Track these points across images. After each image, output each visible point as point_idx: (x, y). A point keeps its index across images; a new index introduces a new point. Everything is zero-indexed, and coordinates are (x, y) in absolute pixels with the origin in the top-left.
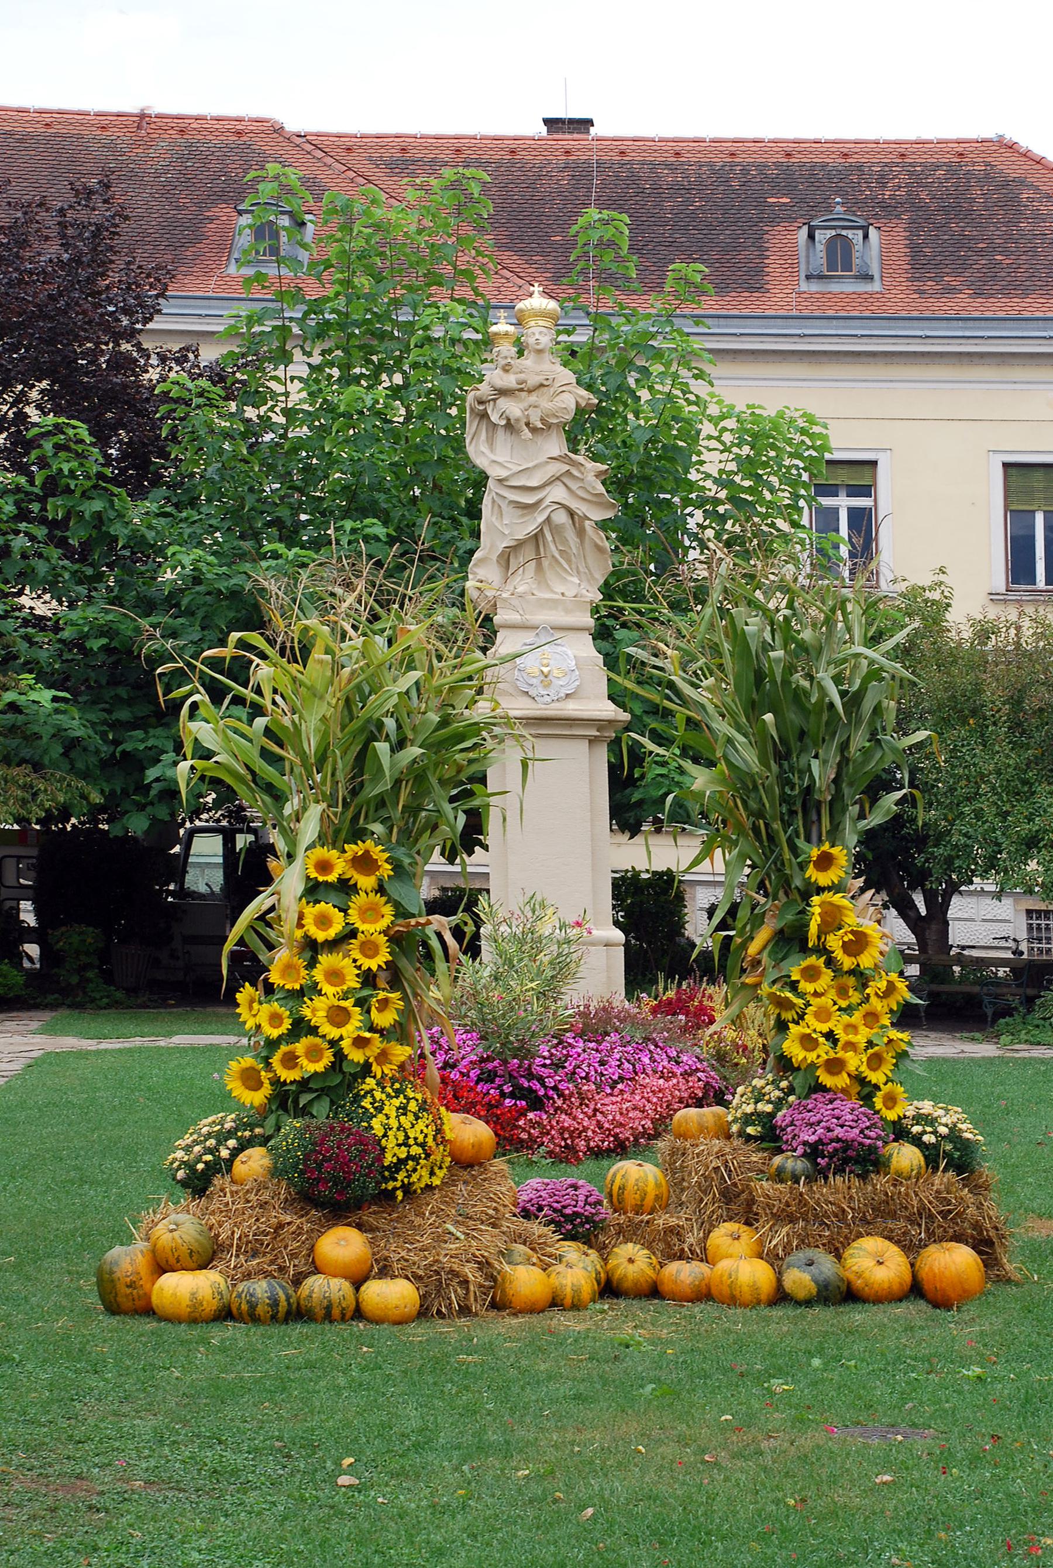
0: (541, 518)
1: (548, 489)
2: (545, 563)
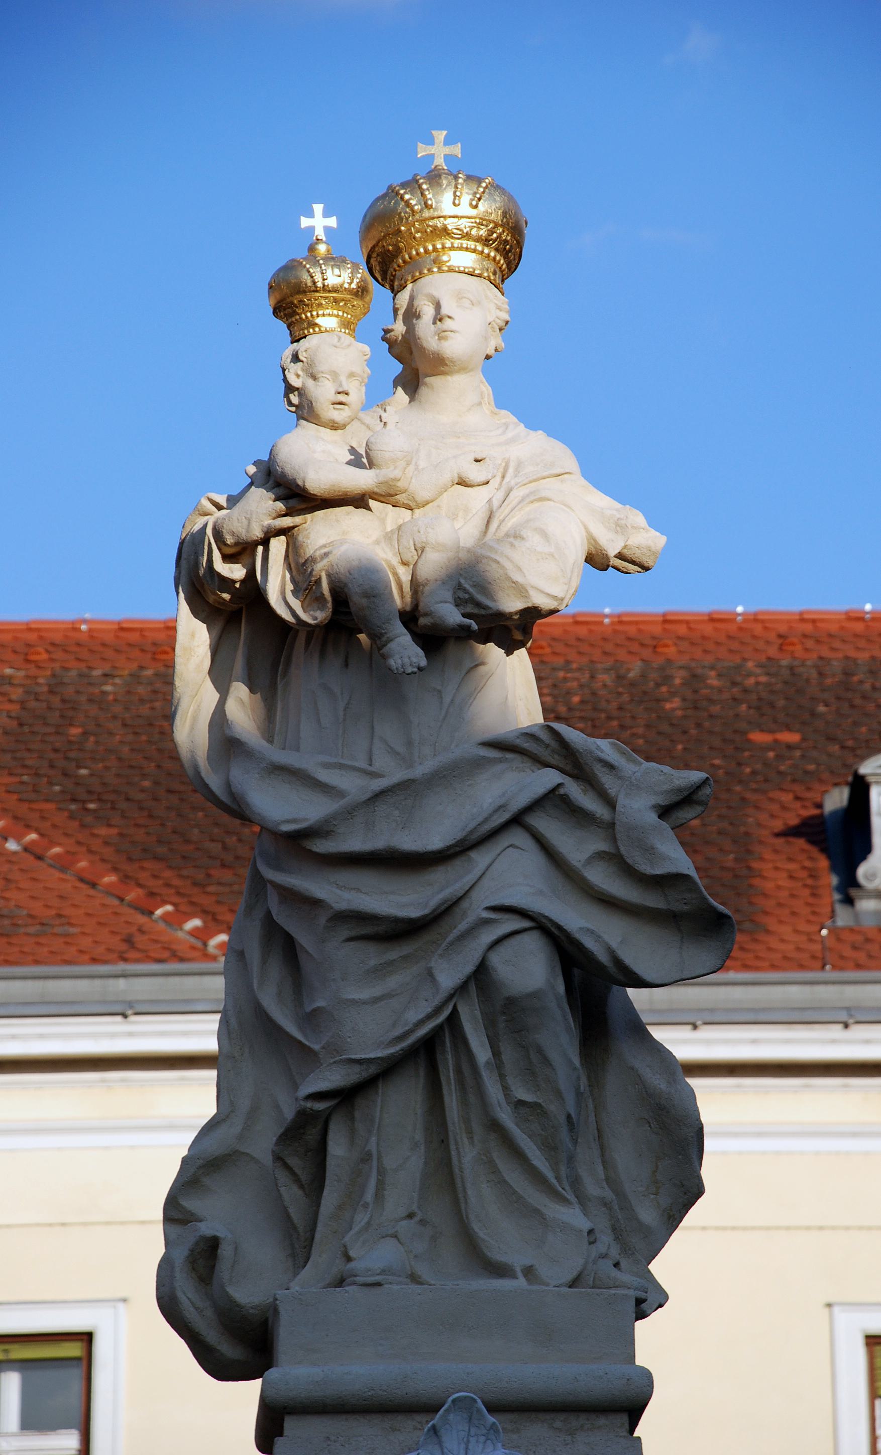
0: (450, 974)
1: (481, 859)
2: (467, 1154)
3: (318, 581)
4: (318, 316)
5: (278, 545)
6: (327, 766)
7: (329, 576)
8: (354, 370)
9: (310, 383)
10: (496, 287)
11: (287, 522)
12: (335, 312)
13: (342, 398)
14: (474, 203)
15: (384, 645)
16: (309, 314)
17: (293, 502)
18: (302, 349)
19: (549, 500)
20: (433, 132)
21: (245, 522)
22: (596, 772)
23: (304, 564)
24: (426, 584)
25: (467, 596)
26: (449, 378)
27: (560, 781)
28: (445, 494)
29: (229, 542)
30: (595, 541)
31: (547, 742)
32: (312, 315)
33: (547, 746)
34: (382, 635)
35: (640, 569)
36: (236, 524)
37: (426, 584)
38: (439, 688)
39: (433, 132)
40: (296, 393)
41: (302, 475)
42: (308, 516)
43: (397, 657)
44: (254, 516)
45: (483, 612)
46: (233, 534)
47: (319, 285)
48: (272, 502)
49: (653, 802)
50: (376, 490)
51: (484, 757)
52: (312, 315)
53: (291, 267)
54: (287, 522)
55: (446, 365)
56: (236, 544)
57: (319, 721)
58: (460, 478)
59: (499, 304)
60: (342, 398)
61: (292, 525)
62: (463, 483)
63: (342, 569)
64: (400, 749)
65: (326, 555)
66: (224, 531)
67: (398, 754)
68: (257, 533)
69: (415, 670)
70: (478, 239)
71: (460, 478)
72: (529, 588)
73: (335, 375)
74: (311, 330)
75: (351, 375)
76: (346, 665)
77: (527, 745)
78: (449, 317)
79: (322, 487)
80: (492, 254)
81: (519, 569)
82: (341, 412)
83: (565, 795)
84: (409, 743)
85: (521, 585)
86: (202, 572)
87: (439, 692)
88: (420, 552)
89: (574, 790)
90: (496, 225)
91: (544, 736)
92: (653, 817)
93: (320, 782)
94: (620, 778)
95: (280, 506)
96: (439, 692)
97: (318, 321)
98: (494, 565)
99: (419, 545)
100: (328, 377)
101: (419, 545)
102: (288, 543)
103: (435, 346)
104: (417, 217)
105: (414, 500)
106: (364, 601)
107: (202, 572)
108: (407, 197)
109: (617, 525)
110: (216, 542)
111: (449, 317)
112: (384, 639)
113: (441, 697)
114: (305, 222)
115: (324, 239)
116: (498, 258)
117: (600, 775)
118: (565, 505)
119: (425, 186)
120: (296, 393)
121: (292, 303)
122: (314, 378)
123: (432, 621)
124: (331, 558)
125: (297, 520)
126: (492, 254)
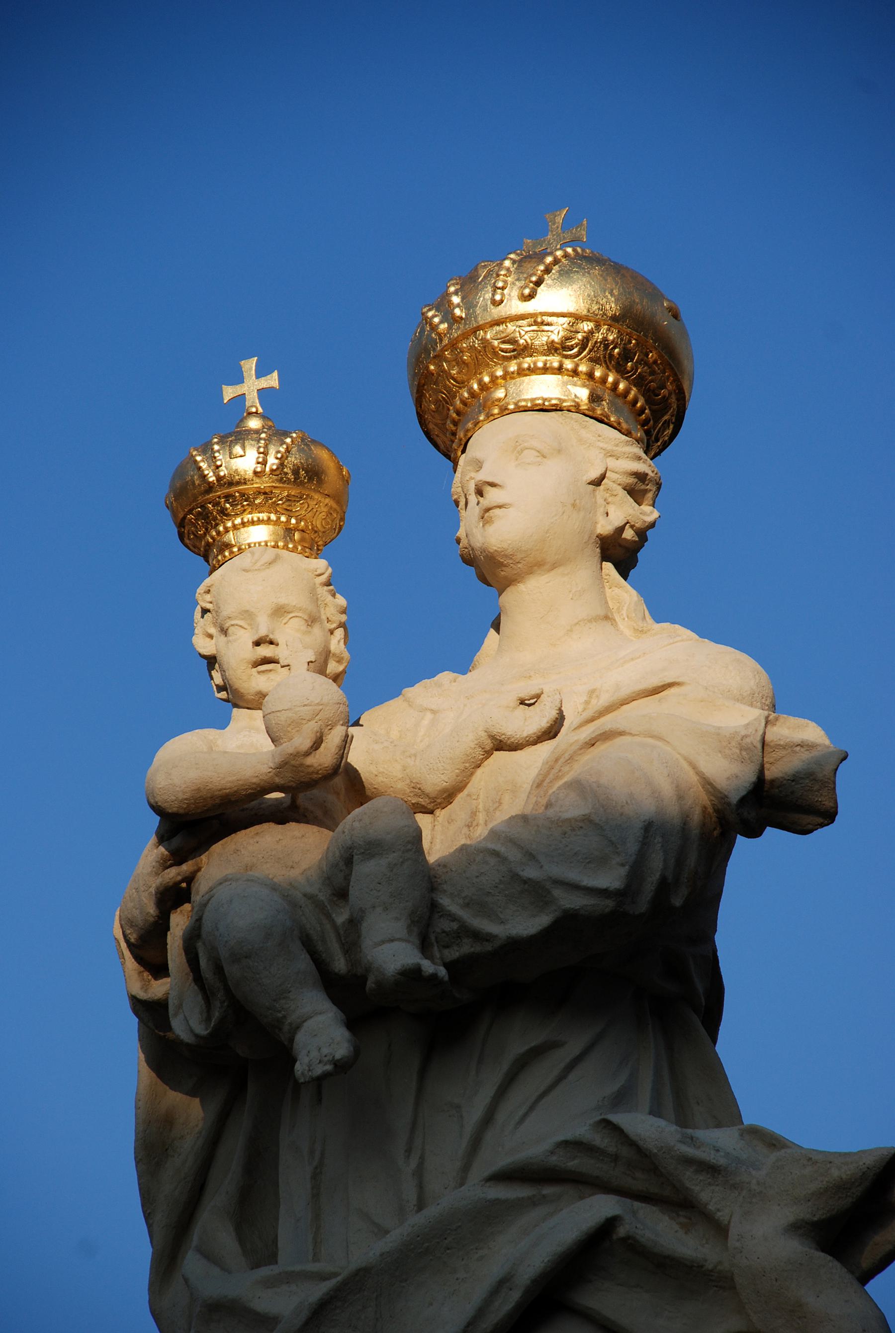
4: (227, 530)
8: (283, 600)
10: (601, 421)
13: (265, 651)
14: (527, 291)
19: (621, 733)
22: (688, 1184)
25: (455, 926)
26: (521, 587)
27: (616, 1211)
28: (479, 771)
30: (710, 784)
31: (612, 1150)
33: (615, 1158)
35: (820, 820)
45: (488, 947)
47: (212, 479)
49: (791, 1219)
51: (497, 1202)
55: (502, 565)
58: (492, 737)
59: (609, 447)
60: (265, 651)
62: (501, 745)
69: (329, 1067)
71: (492, 737)
73: (248, 615)
74: (227, 553)
75: (279, 611)
77: (576, 1163)
78: (493, 485)
79: (181, 796)
80: (583, 368)
82: (271, 675)
83: (628, 1237)
87: (458, 1107)
89: (660, 1230)
90: (578, 318)
91: (600, 1140)
92: (794, 1248)
94: (734, 1187)
96: (458, 1107)
97: (230, 537)
104: (446, 341)
105: (424, 794)
111: (493, 485)
112: (286, 1028)
115: (260, 410)
116: (598, 374)
117: (697, 1189)
118: (652, 737)
126: (583, 368)
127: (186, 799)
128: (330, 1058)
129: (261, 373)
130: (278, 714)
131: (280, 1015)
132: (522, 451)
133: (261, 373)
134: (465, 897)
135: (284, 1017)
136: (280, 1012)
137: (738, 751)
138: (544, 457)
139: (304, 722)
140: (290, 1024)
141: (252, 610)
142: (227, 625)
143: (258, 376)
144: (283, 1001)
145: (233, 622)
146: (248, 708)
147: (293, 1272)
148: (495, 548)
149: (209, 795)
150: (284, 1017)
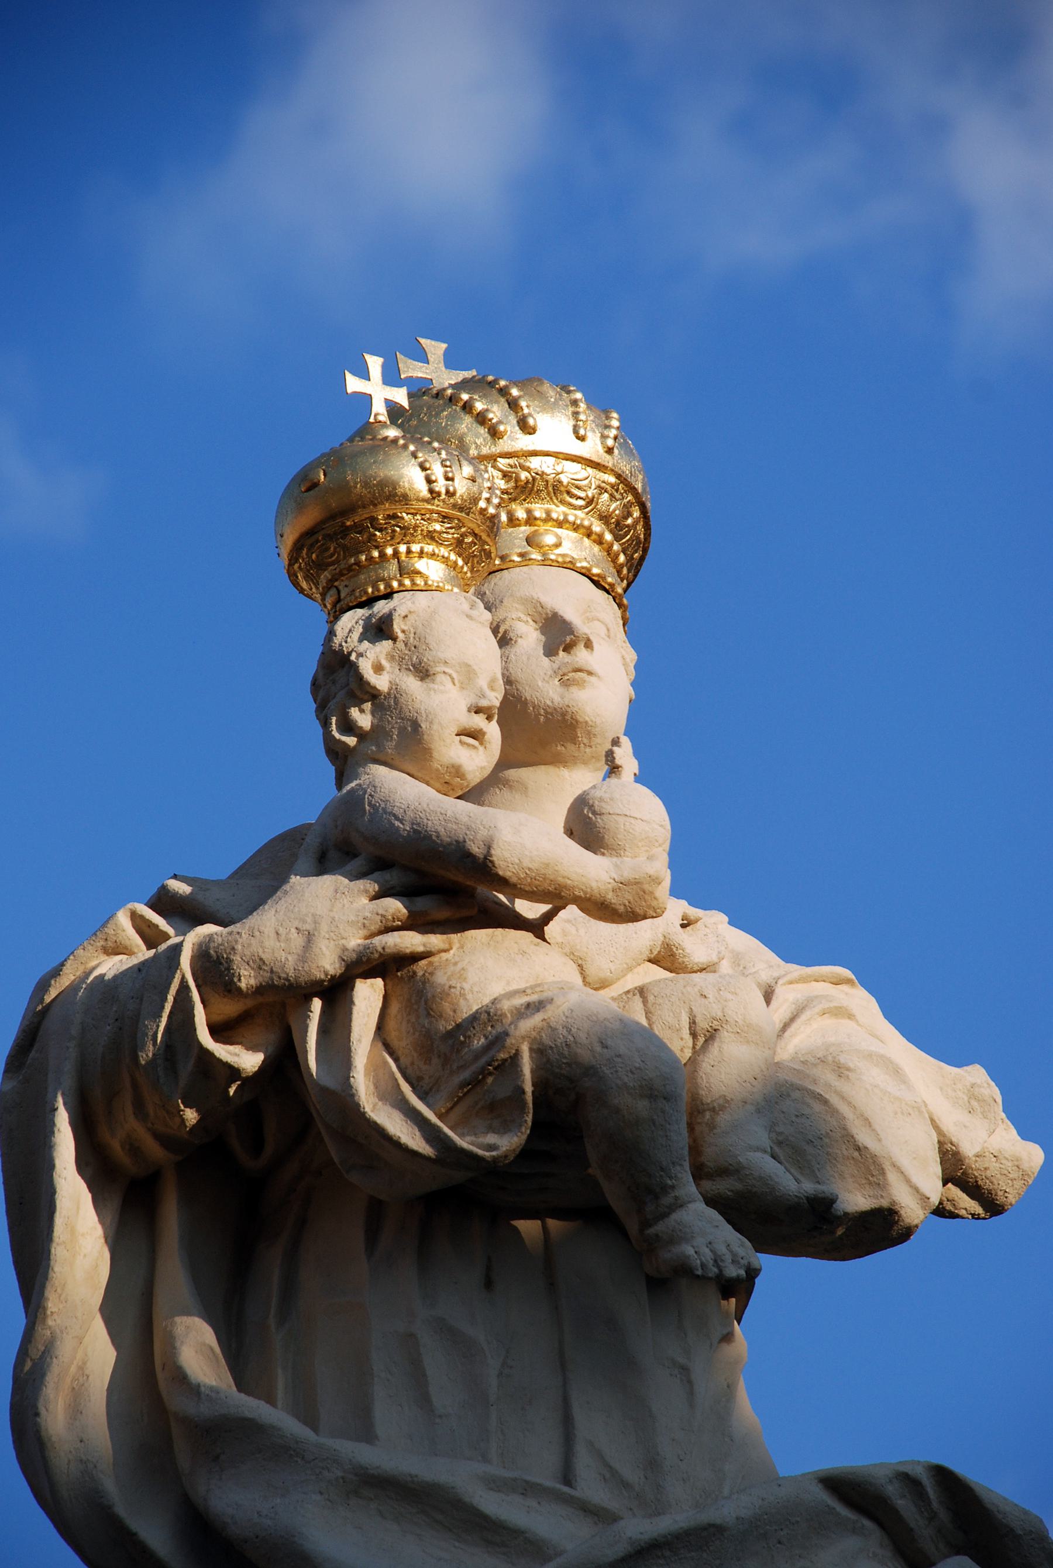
3: (516, 1057)
5: (368, 996)
6: (495, 1484)
7: (540, 1051)
9: (411, 684)
11: (411, 941)
12: (453, 557)
15: (665, 1215)
16: (403, 548)
17: (422, 903)
18: (401, 611)
20: (367, 357)
21: (297, 941)
23: (450, 1034)
24: (722, 1108)
26: (564, 772)
29: (243, 985)
32: (409, 551)
34: (665, 1189)
36: (270, 942)
37: (722, 1108)
38: (681, 1360)
39: (367, 357)
40: (368, 706)
41: (483, 833)
42: (455, 937)
43: (700, 1241)
44: (324, 928)
46: (260, 964)
48: (365, 901)
50: (610, 896)
52: (409, 551)
53: (335, 459)
54: (411, 941)
56: (259, 990)
57: (424, 1400)
61: (421, 949)
63: (582, 1037)
64: (632, 1475)
65: (537, 1006)
66: (237, 958)
67: (626, 1485)
68: (327, 963)
70: (604, 518)
72: (887, 1167)
76: (489, 1284)
79: (526, 863)
81: (868, 1122)
82: (473, 752)
84: (653, 1464)
85: (874, 1157)
86: (147, 1054)
87: (685, 1370)
88: (701, 1040)
93: (485, 1517)
95: (394, 906)
98: (817, 1107)
99: (703, 1024)
100: (455, 675)
101: (703, 1024)
102: (386, 998)
103: (557, 699)
106: (642, 1106)
107: (147, 1054)
108: (479, 406)
109: (972, 1096)
110: (198, 986)
112: (667, 1200)
113: (690, 1382)
114: (354, 384)
119: (515, 392)
120: (368, 706)
121: (373, 520)
122: (423, 673)
123: (739, 1186)
124: (549, 1013)
125: (435, 941)
127: (529, 869)
128: (744, 1262)
129: (364, 373)
130: (632, 821)
131: (669, 1182)
132: (593, 619)
133: (364, 373)
134: (782, 1133)
135: (673, 1187)
136: (671, 1178)
137: (966, 1099)
138: (609, 637)
139: (657, 844)
140: (676, 1198)
141: (475, 667)
142: (438, 669)
143: (368, 378)
144: (678, 1168)
145: (447, 670)
146: (408, 774)
147: (540, 1485)
148: (587, 719)
149: (552, 877)
150: (673, 1187)
